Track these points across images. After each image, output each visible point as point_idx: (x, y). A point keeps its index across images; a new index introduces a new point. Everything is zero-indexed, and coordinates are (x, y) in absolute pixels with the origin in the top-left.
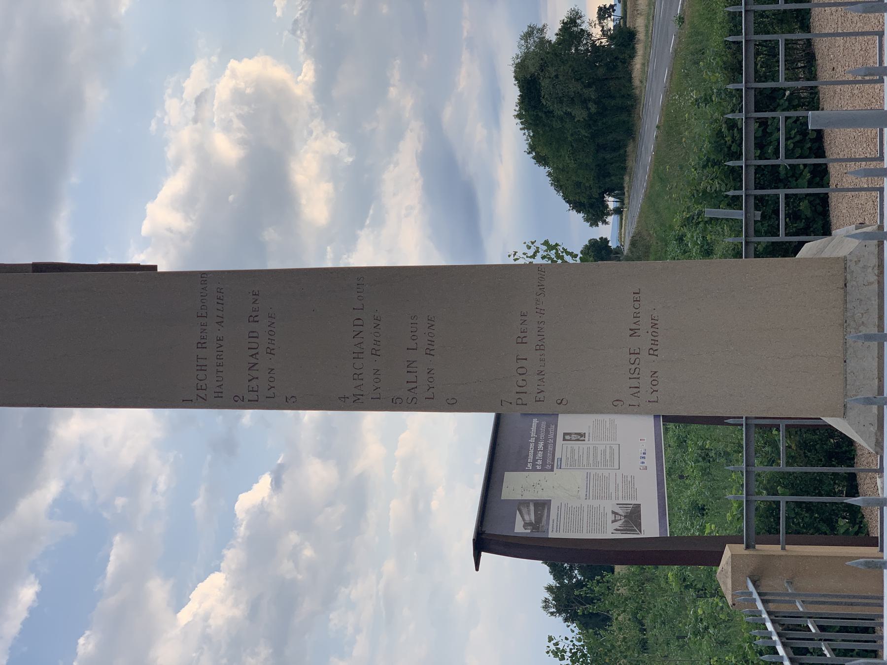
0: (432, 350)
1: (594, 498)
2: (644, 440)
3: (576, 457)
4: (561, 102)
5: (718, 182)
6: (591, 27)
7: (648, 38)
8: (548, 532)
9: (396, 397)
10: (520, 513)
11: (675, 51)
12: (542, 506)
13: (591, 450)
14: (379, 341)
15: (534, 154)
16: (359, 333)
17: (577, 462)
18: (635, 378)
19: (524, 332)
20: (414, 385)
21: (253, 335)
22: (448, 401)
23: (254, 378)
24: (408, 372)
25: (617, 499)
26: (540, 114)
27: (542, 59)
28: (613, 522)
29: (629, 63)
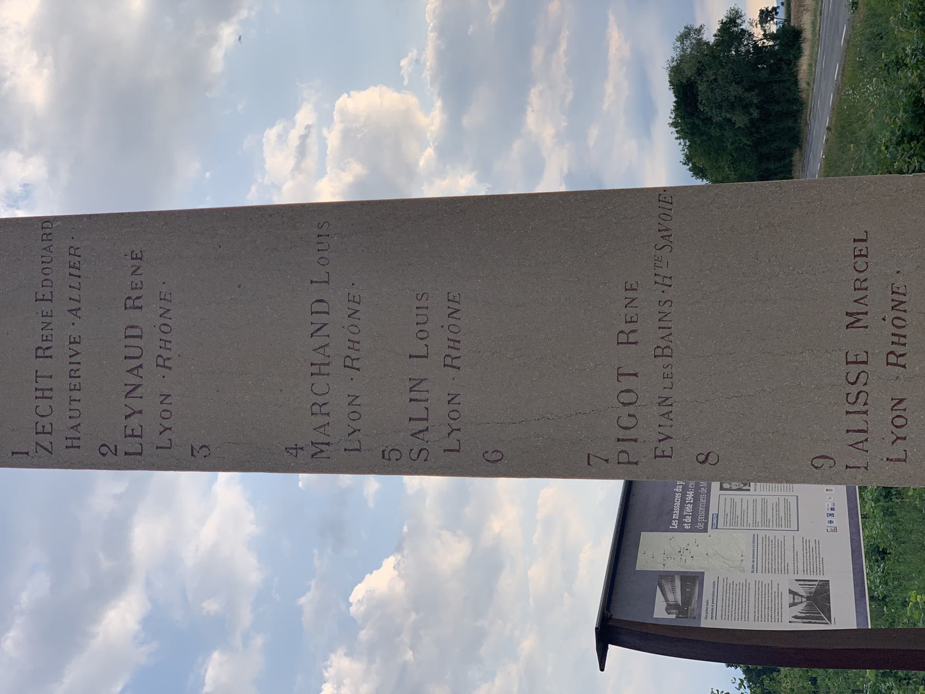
0: (456, 358)
1: (764, 571)
2: (832, 490)
3: (738, 513)
4: (720, 107)
5: (917, 159)
6: (752, 27)
7: (816, 36)
8: (700, 618)
9: (390, 448)
10: (661, 591)
11: (847, 41)
12: (692, 580)
13: (759, 502)
14: (358, 343)
15: (691, 165)
16: (321, 328)
17: (739, 519)
18: (858, 412)
20: (422, 425)
21: (132, 333)
23: (134, 413)
24: (411, 400)
25: (796, 572)
26: (696, 121)
27: (699, 62)
28: (791, 605)
29: (795, 65)
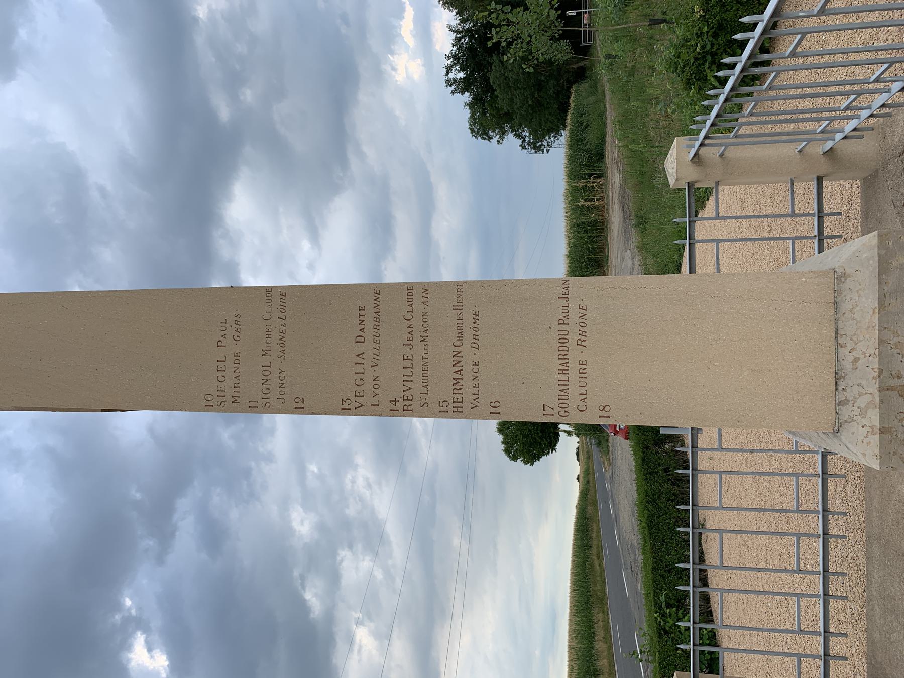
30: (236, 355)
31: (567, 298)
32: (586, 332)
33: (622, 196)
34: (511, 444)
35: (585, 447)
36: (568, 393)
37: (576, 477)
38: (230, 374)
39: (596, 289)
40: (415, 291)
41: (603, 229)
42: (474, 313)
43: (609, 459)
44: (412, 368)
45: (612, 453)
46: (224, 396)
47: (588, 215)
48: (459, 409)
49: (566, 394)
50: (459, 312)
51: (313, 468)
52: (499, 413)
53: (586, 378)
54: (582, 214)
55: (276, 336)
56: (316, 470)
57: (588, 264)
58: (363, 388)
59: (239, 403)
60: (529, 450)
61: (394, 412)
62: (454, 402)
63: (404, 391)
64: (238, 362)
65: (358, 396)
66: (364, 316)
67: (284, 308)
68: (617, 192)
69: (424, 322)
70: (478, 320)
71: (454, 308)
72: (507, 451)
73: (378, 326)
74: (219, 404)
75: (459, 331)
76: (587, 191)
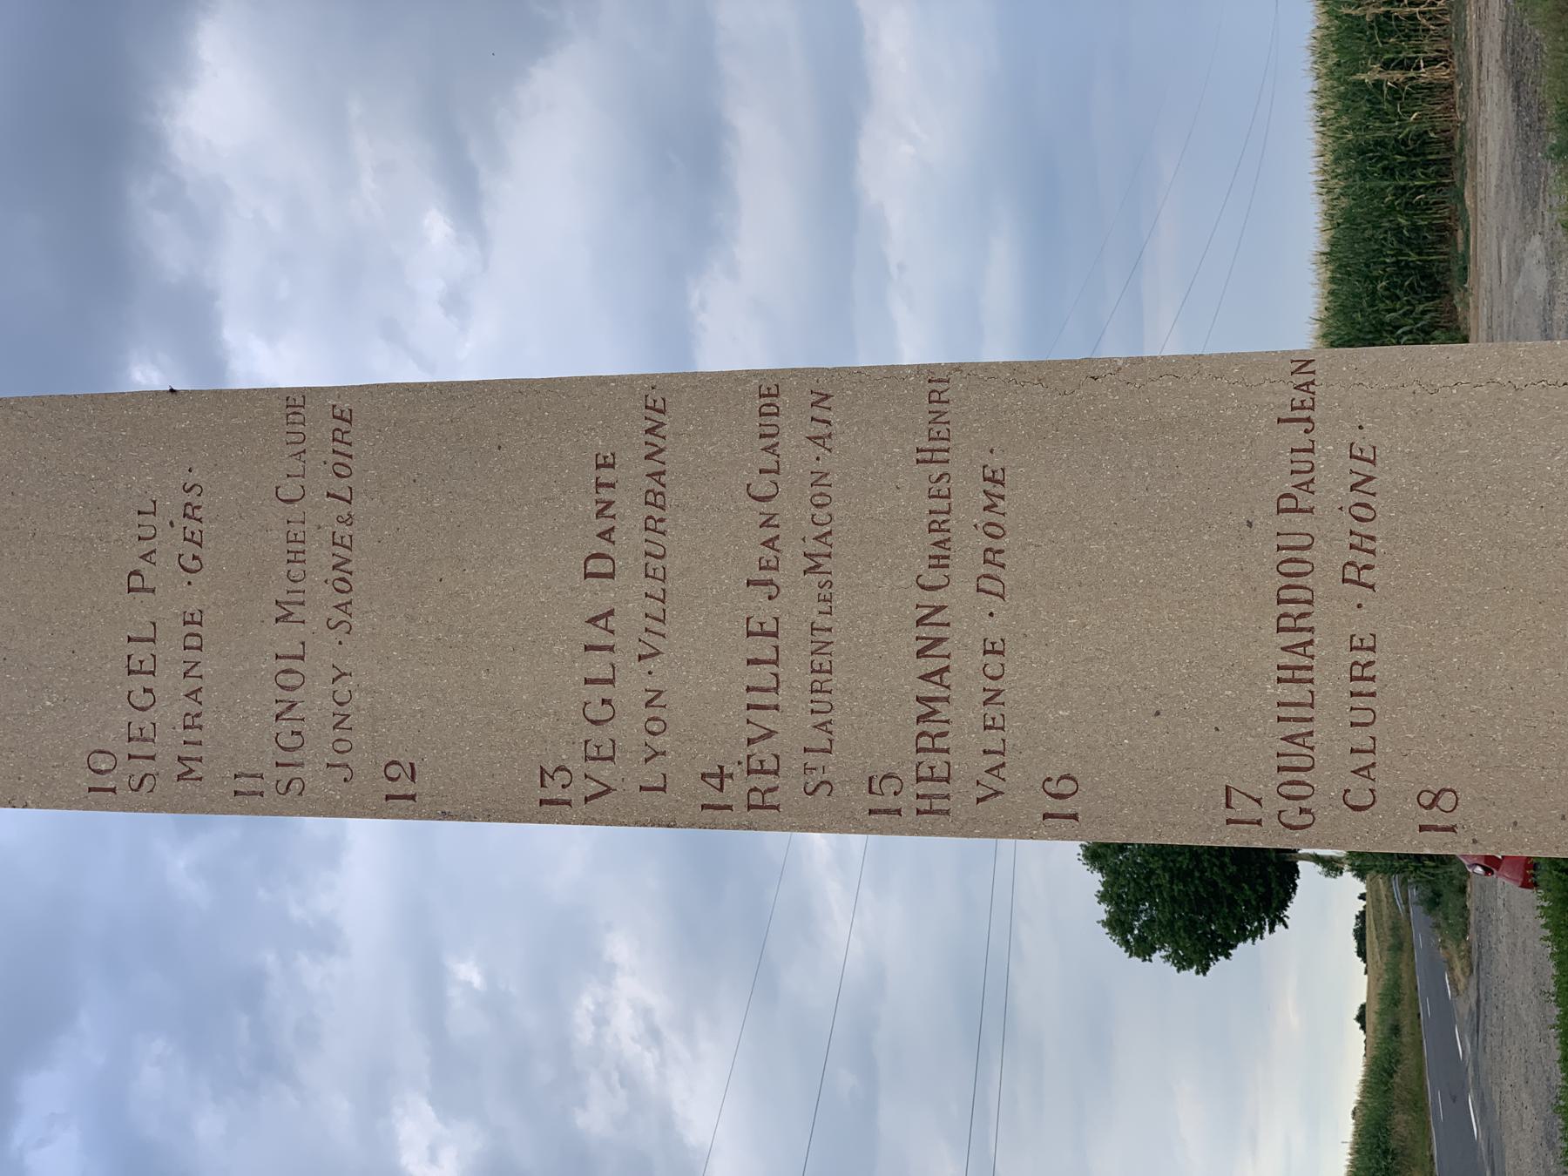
19: (139, 672)
22: (1051, 787)
30: (188, 618)
31: (1308, 420)
32: (1372, 538)
33: (1513, 53)
34: (1129, 903)
35: (1385, 912)
36: (1312, 748)
37: (1356, 1012)
38: (169, 680)
39: (1409, 389)
40: (784, 401)
41: (1447, 162)
42: (989, 474)
43: (1469, 952)
44: (775, 662)
45: (1478, 931)
46: (153, 758)
47: (1396, 114)
48: (938, 804)
49: (1305, 751)
50: (937, 470)
51: (468, 972)
52: (1075, 817)
53: (1373, 694)
54: (1376, 112)
55: (320, 556)
56: (477, 980)
57: (1395, 285)
58: (610, 730)
59: (200, 779)
60: (1193, 922)
61: (714, 813)
62: (919, 780)
63: (750, 742)
64: (194, 642)
65: (594, 759)
66: (613, 486)
67: (347, 461)
68: (1497, 36)
69: (817, 506)
70: (1002, 497)
71: (920, 456)
72: (1118, 925)
73: (661, 520)
74: (135, 784)
75: (938, 537)
76: (1391, 33)
